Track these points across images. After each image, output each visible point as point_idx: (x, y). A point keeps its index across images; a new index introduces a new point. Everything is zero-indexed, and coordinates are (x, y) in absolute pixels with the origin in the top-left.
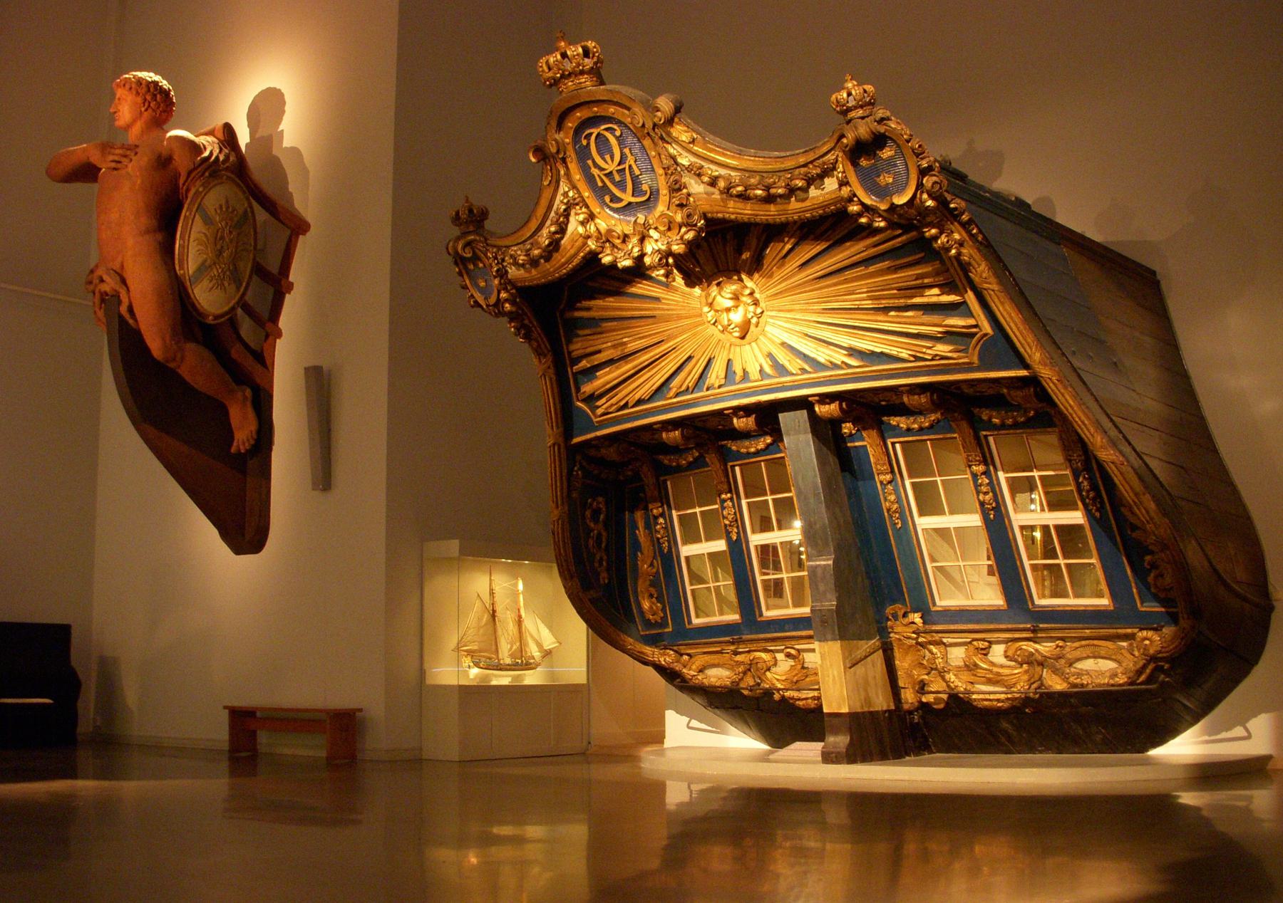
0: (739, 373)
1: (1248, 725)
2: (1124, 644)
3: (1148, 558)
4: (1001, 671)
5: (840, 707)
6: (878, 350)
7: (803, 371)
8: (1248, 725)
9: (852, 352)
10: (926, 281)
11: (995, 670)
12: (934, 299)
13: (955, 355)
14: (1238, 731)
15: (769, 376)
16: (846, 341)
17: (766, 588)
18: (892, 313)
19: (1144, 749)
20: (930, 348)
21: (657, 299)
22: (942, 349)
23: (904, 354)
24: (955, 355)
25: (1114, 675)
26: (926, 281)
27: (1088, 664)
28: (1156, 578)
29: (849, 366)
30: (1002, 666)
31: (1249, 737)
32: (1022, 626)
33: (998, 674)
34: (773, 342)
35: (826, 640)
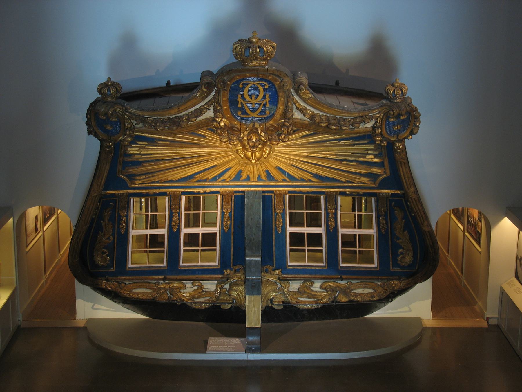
0: (244, 176)
1: (410, 306)
2: (379, 283)
3: (401, 250)
4: (316, 294)
5: (256, 325)
6: (331, 177)
7: (284, 180)
8: (410, 306)
9: (316, 176)
10: (369, 152)
11: (313, 293)
12: (370, 160)
13: (369, 183)
14: (406, 309)
15: (262, 180)
16: (314, 171)
17: (162, 244)
18: (345, 162)
19: (362, 316)
20: (358, 179)
21: (205, 137)
22: (363, 179)
23: (343, 179)
24: (369, 183)
25: (373, 296)
26: (369, 152)
27: (360, 291)
28: (402, 258)
29: (312, 182)
30: (316, 292)
31: (410, 311)
32: (333, 276)
33: (315, 295)
34: (272, 166)
35: (253, 294)
